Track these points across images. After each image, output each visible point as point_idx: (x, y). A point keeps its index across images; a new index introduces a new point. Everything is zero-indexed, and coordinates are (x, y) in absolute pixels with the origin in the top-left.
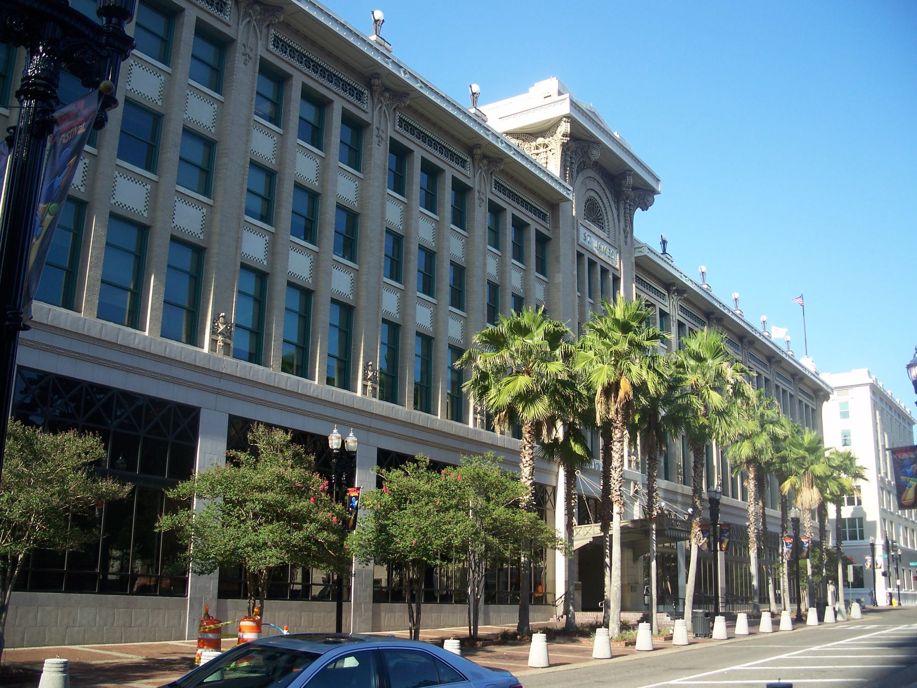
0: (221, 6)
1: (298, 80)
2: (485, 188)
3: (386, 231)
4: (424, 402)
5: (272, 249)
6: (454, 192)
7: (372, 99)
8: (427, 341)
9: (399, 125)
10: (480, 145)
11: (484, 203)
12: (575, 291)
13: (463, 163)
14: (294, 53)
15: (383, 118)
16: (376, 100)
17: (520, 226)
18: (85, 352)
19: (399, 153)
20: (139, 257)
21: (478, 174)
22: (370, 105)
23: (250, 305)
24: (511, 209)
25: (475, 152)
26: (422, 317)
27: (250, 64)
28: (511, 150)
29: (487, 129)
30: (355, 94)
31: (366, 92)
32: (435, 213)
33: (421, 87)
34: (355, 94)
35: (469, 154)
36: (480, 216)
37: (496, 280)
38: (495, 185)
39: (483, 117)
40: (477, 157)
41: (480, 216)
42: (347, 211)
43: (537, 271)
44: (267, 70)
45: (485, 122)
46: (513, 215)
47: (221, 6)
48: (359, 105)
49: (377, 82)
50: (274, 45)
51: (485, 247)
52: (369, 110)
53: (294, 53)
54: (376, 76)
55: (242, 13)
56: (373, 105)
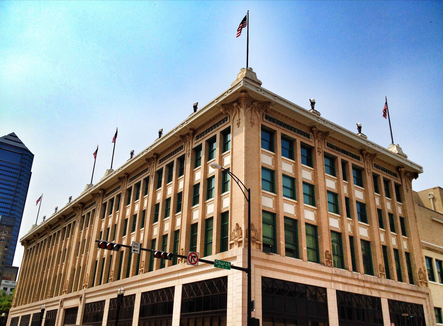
0: (308, 136)
1: (279, 131)
2: (370, 167)
3: (327, 192)
4: (400, 279)
5: (276, 204)
6: (355, 171)
7: (363, 158)
8: (367, 244)
9: (327, 146)
10: (315, 126)
11: (370, 174)
12: (259, 147)
13: (358, 158)
14: (292, 128)
15: (320, 145)
16: (365, 159)
17: (387, 182)
18: (325, 278)
19: (375, 178)
20: (340, 244)
21: (366, 162)
22: (313, 139)
23: (311, 239)
24: (382, 175)
25: (313, 130)
26: (393, 242)
27: (370, 175)
28: (333, 126)
29: (368, 142)
30: (272, 120)
31: (311, 134)
32: (363, 187)
33: (263, 93)
34: (272, 120)
35: (311, 131)
36: (320, 160)
37: (380, 208)
38: (374, 165)
39: (365, 136)
40: (314, 132)
41: (320, 160)
42: (270, 171)
43: (397, 201)
44: (326, 156)
45: (366, 138)
46: (383, 177)
47: (308, 136)
48: (308, 140)
49: (315, 129)
50: (266, 118)
51: (374, 193)
52: (313, 141)
53: (292, 128)
54: (314, 126)
55: (315, 137)
56: (315, 139)
